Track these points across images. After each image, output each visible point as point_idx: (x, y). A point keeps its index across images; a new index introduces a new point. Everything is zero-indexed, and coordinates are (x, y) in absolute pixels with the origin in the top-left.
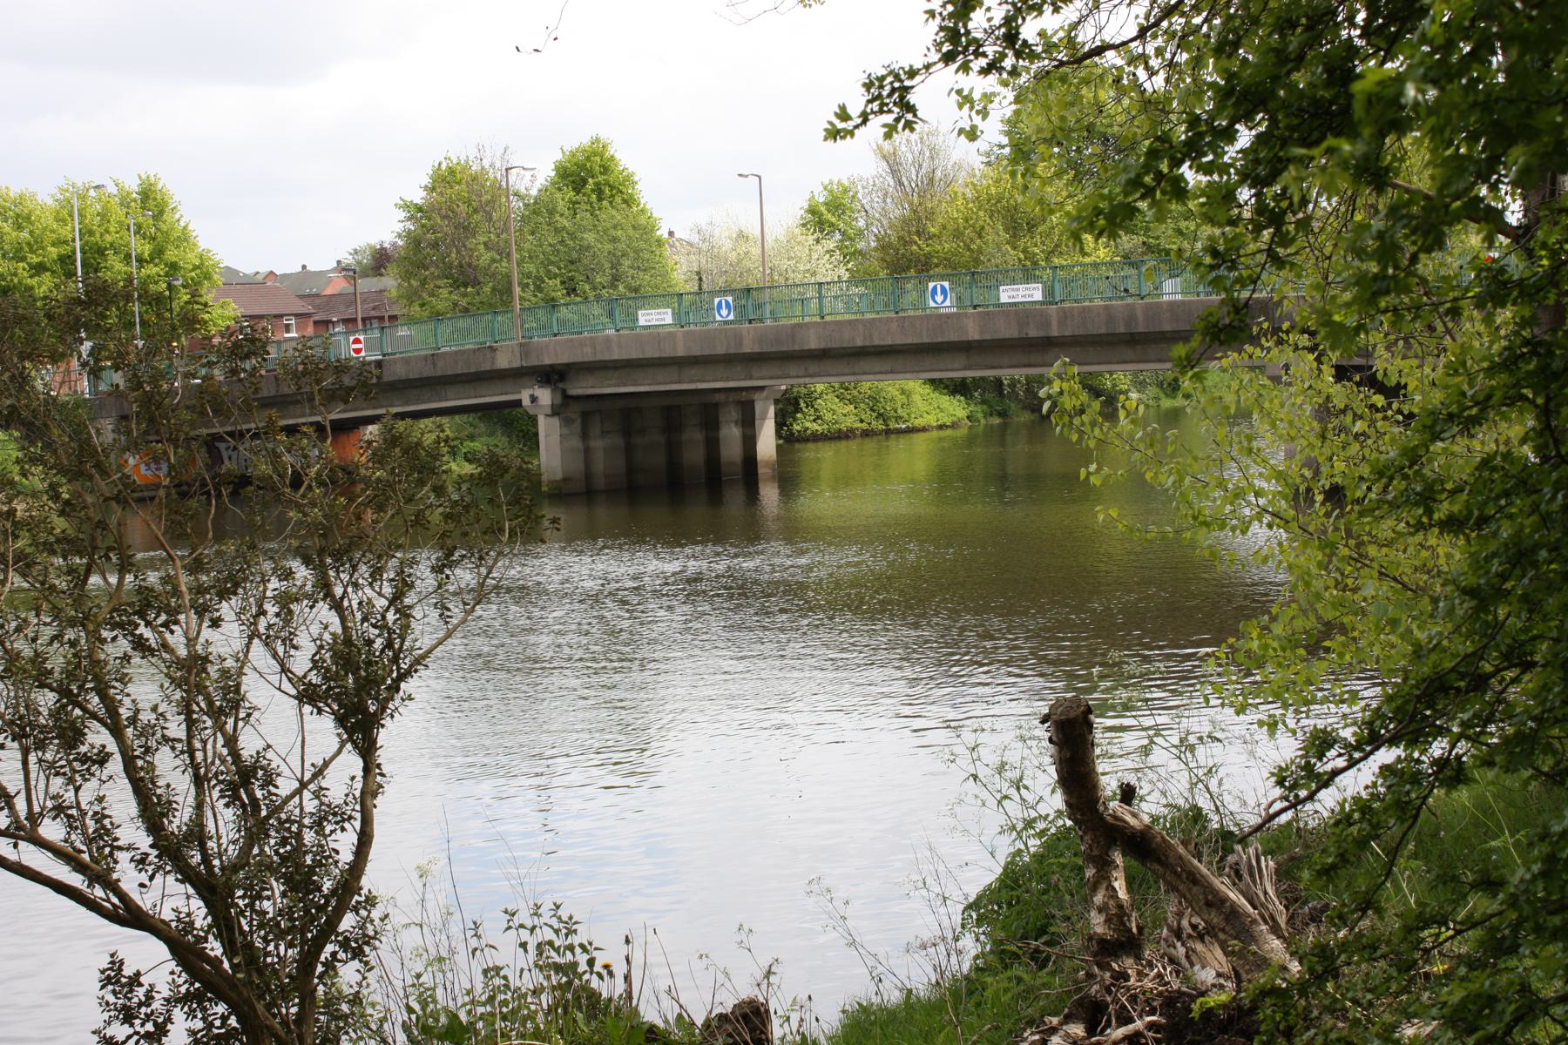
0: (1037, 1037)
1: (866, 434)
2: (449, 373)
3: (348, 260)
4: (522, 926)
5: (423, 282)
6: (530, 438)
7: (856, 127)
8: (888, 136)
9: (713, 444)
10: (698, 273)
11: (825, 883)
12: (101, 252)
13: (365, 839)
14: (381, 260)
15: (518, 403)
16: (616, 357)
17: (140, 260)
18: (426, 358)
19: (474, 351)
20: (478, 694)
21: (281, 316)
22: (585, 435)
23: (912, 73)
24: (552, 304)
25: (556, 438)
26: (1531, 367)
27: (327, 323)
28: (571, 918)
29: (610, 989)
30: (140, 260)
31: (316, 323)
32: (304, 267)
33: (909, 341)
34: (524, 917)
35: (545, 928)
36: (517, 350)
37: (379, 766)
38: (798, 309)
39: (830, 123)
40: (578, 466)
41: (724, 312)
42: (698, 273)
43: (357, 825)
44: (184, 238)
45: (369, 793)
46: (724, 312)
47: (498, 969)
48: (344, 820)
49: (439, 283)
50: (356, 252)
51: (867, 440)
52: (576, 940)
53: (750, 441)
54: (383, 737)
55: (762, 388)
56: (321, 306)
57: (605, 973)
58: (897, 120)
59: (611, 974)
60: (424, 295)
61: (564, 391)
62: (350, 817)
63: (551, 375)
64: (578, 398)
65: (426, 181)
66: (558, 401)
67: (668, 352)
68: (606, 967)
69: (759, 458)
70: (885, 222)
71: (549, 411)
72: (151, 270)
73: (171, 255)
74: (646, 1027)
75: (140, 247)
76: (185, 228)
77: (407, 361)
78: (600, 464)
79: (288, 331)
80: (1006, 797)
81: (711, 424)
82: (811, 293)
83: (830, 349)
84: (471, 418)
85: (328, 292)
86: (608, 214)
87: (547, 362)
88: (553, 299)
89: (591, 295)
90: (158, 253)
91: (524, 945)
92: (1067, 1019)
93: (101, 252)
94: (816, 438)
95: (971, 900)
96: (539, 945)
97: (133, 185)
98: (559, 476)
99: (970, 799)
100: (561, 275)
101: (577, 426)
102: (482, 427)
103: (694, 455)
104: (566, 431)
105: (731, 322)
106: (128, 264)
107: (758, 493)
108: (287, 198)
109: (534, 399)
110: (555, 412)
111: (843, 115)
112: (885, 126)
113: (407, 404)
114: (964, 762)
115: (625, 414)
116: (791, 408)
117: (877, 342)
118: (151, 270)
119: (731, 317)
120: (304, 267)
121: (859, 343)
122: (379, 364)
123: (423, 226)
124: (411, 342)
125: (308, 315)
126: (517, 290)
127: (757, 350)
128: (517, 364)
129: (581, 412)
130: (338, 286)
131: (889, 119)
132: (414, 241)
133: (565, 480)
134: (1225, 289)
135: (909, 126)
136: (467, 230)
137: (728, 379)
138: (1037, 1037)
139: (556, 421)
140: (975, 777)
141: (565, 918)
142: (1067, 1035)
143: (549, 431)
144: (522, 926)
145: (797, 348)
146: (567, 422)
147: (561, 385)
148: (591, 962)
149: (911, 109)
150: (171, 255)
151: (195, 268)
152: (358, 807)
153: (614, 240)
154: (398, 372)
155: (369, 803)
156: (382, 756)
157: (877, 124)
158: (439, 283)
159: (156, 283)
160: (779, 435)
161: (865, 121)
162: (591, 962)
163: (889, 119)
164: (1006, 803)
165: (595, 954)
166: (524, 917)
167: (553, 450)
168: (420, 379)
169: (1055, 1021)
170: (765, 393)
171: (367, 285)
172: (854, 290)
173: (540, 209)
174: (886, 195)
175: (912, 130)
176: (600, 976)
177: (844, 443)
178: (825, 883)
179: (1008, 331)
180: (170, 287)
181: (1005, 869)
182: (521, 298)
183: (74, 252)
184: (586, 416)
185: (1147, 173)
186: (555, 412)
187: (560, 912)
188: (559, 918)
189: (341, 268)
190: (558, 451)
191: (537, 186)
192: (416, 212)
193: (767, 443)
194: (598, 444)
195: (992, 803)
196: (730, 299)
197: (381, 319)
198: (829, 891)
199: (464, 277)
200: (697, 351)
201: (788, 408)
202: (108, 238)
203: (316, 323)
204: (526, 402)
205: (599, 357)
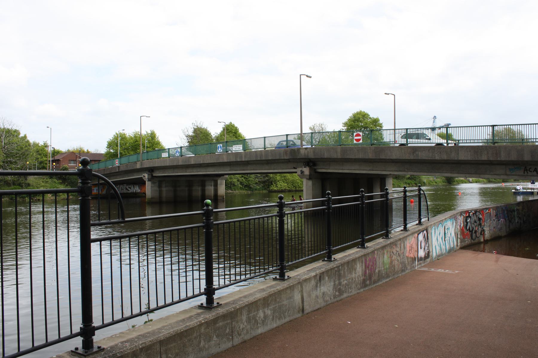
20: (310, 249)
22: (160, 186)
25: (150, 187)
26: (23, 208)
40: (157, 195)
41: (220, 149)
46: (220, 149)
61: (152, 175)
63: (151, 170)
64: (156, 177)
66: (150, 177)
81: (203, 186)
97: (149, 132)
98: (150, 197)
101: (157, 184)
104: (153, 185)
115: (174, 181)
117: (205, 162)
129: (159, 181)
133: (152, 198)
139: (150, 183)
146: (153, 183)
179: (233, 159)
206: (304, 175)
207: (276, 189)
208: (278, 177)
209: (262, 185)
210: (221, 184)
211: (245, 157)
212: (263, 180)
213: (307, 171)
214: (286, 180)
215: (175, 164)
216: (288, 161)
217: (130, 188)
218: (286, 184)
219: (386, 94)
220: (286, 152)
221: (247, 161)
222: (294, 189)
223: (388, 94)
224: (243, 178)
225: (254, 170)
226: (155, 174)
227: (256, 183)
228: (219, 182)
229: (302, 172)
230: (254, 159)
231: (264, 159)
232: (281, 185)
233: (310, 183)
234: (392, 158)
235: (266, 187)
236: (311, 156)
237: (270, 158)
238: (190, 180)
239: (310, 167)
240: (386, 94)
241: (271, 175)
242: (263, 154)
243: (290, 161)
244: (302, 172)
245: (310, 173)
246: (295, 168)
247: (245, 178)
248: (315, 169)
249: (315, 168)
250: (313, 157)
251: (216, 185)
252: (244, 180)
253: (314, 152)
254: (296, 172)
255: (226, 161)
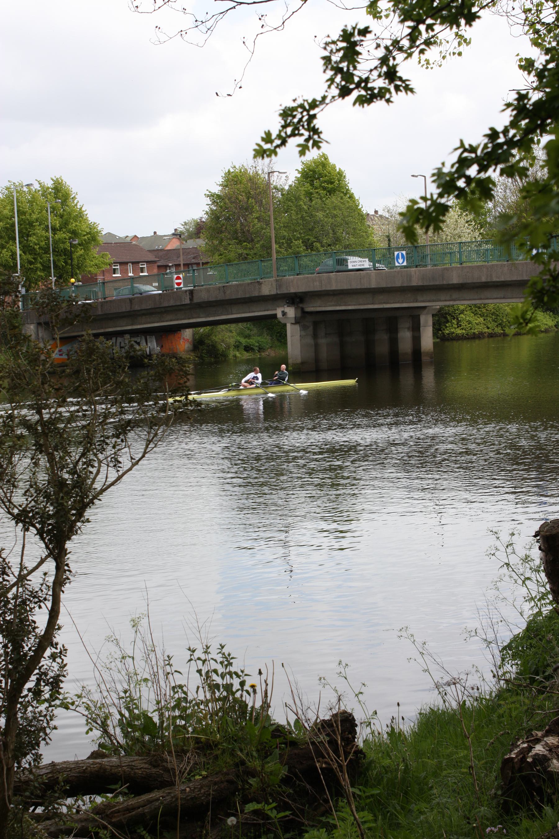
0: (525, 745)
1: (491, 336)
2: (234, 297)
3: (181, 228)
4: (199, 659)
5: (221, 241)
6: (280, 336)
7: (278, 146)
8: (302, 153)
9: (394, 342)
10: (388, 237)
11: (410, 632)
12: (31, 224)
13: (54, 614)
14: (199, 229)
15: (275, 316)
16: (334, 288)
17: (54, 230)
18: (219, 288)
19: (248, 284)
21: (138, 262)
22: (315, 336)
23: (314, 105)
24: (297, 256)
25: (298, 337)
27: (166, 267)
28: (229, 655)
29: (254, 702)
30: (54, 230)
31: (159, 267)
32: (155, 233)
33: (515, 278)
34: (199, 653)
35: (212, 661)
36: (274, 284)
37: (67, 565)
38: (447, 259)
39: (258, 145)
41: (401, 261)
42: (388, 237)
43: (49, 604)
44: (80, 216)
45: (59, 583)
46: (401, 261)
47: (181, 687)
48: (40, 601)
49: (230, 242)
50: (186, 224)
51: (491, 339)
52: (233, 669)
53: (417, 340)
54: (69, 545)
55: (424, 308)
56: (157, 257)
57: (251, 690)
58: (307, 140)
59: (255, 692)
60: (222, 249)
61: (302, 309)
62: (45, 599)
63: (295, 299)
65: (220, 180)
66: (299, 314)
67: (365, 285)
68: (253, 686)
69: (422, 350)
70: (506, 205)
71: (293, 321)
72: (60, 235)
73: (73, 226)
74: (272, 728)
75: (51, 220)
76: (81, 209)
77: (208, 290)
78: (324, 354)
79: (142, 272)
80: (528, 579)
82: (456, 249)
83: (465, 284)
84: (249, 325)
85: (169, 248)
86: (334, 200)
87: (293, 290)
88: (298, 253)
89: (321, 249)
90: (65, 224)
91: (199, 671)
92: (548, 733)
93: (31, 224)
94: (459, 338)
95: (505, 644)
96: (208, 672)
97: (49, 184)
98: (299, 361)
99: (507, 578)
100: (301, 238)
102: (255, 331)
103: (382, 348)
104: (303, 333)
105: (405, 267)
106: (47, 231)
107: (421, 371)
108: (145, 192)
109: (284, 314)
110: (297, 321)
111: (268, 138)
112: (299, 146)
113: (208, 316)
114: (502, 556)
115: (340, 323)
116: (443, 320)
117: (495, 279)
118: (60, 235)
119: (405, 264)
120: (155, 233)
121: (484, 279)
122: (191, 292)
123: (221, 207)
124: (213, 280)
125: (154, 262)
126: (275, 246)
127: (420, 284)
128: (274, 292)
129: (311, 321)
130: (175, 244)
131: (300, 140)
132: (214, 216)
133: (303, 363)
134: (543, 263)
135: (316, 144)
136: (248, 209)
137: (402, 302)
138: (525, 745)
139: (297, 327)
140: (508, 565)
141: (226, 654)
142: (547, 744)
143: (293, 333)
144: (199, 659)
145: (445, 283)
146: (304, 328)
147: (301, 305)
148: (242, 684)
149: (315, 131)
150: (73, 226)
151: (88, 234)
152: (50, 593)
153: (335, 216)
154: (202, 297)
155: (57, 590)
156: (72, 560)
157: (293, 142)
158: (230, 242)
159: (64, 243)
160: (435, 335)
161: (284, 143)
162: (242, 684)
163: (300, 140)
164: (528, 582)
165: (246, 678)
166: (199, 653)
167: (295, 342)
168: (216, 302)
169: (540, 734)
170: (425, 311)
171: (191, 244)
172: (485, 247)
173: (291, 196)
174: (506, 188)
175: (319, 148)
176: (248, 692)
177: (477, 341)
178: (410, 632)
180: (72, 245)
181: (529, 624)
182: (278, 252)
183: (13, 225)
184: (316, 325)
185: (459, 178)
186: (297, 321)
187: (224, 650)
188: (224, 654)
189: (177, 235)
190: (299, 345)
191: (290, 182)
192: (214, 198)
193: (427, 340)
194: (323, 341)
195: (520, 582)
196: (404, 252)
197: (198, 264)
198: (412, 636)
199: (244, 237)
200: (383, 285)
201: (441, 319)
202: (34, 216)
203: (159, 267)
204: (279, 315)
205: (324, 289)
207: (459, 331)
217: (139, 344)
219: (413, 176)
223: (417, 176)
226: (310, 308)
234: (451, 283)
238: (369, 322)
240: (413, 176)
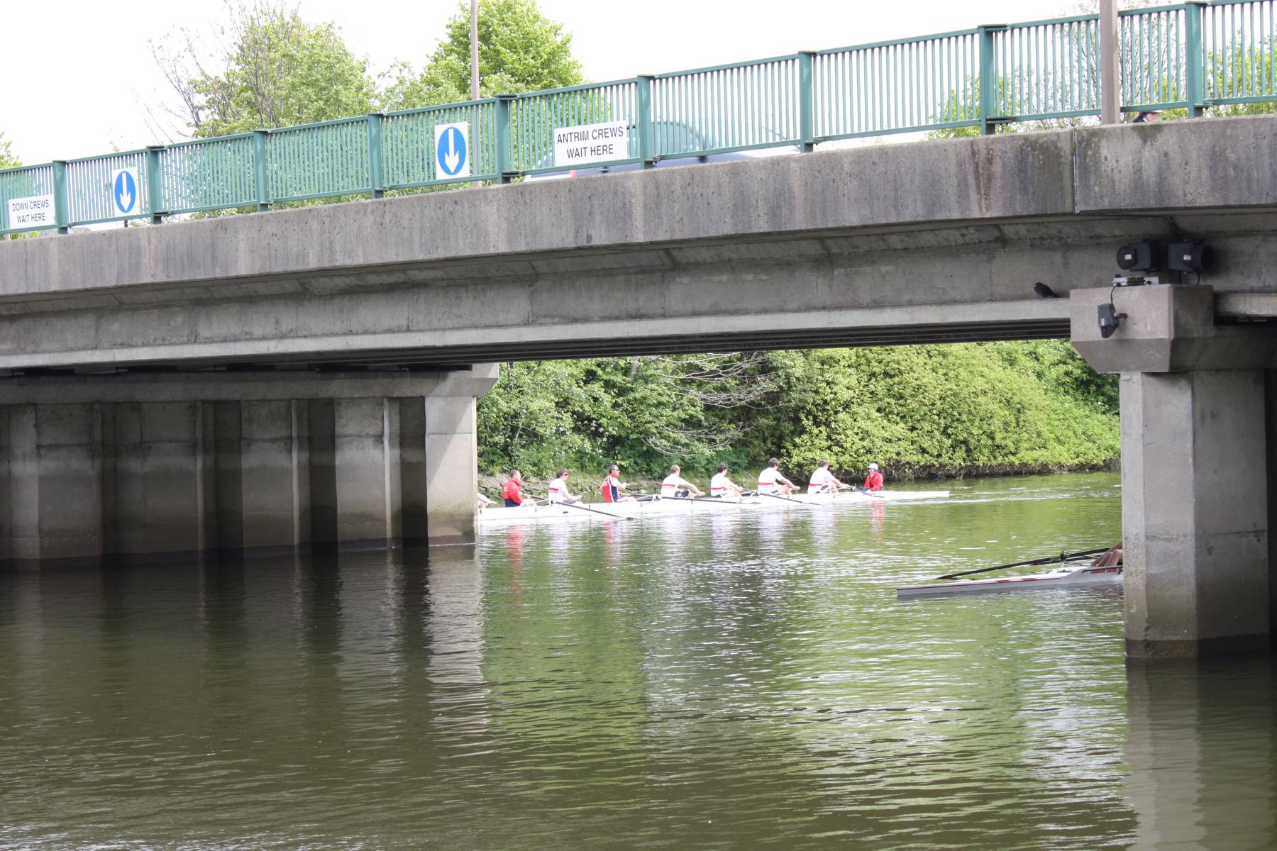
40: (83, 509)
81: (319, 437)
117: (342, 261)
179: (555, 233)
206: (1123, 342)
208: (842, 373)
209: (734, 432)
210: (450, 428)
211: (653, 211)
212: (743, 396)
213: (1151, 309)
214: (897, 404)
215: (109, 281)
216: (989, 239)
218: (900, 429)
220: (978, 166)
221: (668, 248)
222: (959, 459)
224: (597, 388)
225: (716, 312)
227: (691, 423)
228: (434, 410)
229: (1114, 322)
230: (726, 228)
231: (799, 222)
232: (865, 435)
233: (1178, 404)
235: (758, 448)
236: (1194, 189)
237: (851, 218)
238: (223, 402)
239: (1168, 275)
241: (794, 362)
242: (796, 184)
243: (1003, 241)
244: (1114, 322)
245: (1177, 324)
246: (1045, 292)
247: (608, 385)
248: (1217, 297)
249: (1218, 284)
250: (1203, 197)
251: (412, 437)
252: (607, 400)
253: (1216, 158)
254: (1059, 329)
255: (503, 248)
